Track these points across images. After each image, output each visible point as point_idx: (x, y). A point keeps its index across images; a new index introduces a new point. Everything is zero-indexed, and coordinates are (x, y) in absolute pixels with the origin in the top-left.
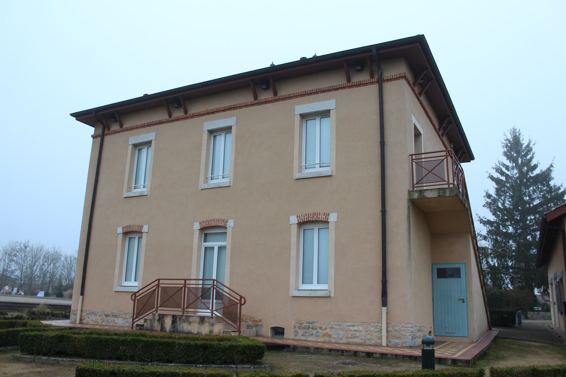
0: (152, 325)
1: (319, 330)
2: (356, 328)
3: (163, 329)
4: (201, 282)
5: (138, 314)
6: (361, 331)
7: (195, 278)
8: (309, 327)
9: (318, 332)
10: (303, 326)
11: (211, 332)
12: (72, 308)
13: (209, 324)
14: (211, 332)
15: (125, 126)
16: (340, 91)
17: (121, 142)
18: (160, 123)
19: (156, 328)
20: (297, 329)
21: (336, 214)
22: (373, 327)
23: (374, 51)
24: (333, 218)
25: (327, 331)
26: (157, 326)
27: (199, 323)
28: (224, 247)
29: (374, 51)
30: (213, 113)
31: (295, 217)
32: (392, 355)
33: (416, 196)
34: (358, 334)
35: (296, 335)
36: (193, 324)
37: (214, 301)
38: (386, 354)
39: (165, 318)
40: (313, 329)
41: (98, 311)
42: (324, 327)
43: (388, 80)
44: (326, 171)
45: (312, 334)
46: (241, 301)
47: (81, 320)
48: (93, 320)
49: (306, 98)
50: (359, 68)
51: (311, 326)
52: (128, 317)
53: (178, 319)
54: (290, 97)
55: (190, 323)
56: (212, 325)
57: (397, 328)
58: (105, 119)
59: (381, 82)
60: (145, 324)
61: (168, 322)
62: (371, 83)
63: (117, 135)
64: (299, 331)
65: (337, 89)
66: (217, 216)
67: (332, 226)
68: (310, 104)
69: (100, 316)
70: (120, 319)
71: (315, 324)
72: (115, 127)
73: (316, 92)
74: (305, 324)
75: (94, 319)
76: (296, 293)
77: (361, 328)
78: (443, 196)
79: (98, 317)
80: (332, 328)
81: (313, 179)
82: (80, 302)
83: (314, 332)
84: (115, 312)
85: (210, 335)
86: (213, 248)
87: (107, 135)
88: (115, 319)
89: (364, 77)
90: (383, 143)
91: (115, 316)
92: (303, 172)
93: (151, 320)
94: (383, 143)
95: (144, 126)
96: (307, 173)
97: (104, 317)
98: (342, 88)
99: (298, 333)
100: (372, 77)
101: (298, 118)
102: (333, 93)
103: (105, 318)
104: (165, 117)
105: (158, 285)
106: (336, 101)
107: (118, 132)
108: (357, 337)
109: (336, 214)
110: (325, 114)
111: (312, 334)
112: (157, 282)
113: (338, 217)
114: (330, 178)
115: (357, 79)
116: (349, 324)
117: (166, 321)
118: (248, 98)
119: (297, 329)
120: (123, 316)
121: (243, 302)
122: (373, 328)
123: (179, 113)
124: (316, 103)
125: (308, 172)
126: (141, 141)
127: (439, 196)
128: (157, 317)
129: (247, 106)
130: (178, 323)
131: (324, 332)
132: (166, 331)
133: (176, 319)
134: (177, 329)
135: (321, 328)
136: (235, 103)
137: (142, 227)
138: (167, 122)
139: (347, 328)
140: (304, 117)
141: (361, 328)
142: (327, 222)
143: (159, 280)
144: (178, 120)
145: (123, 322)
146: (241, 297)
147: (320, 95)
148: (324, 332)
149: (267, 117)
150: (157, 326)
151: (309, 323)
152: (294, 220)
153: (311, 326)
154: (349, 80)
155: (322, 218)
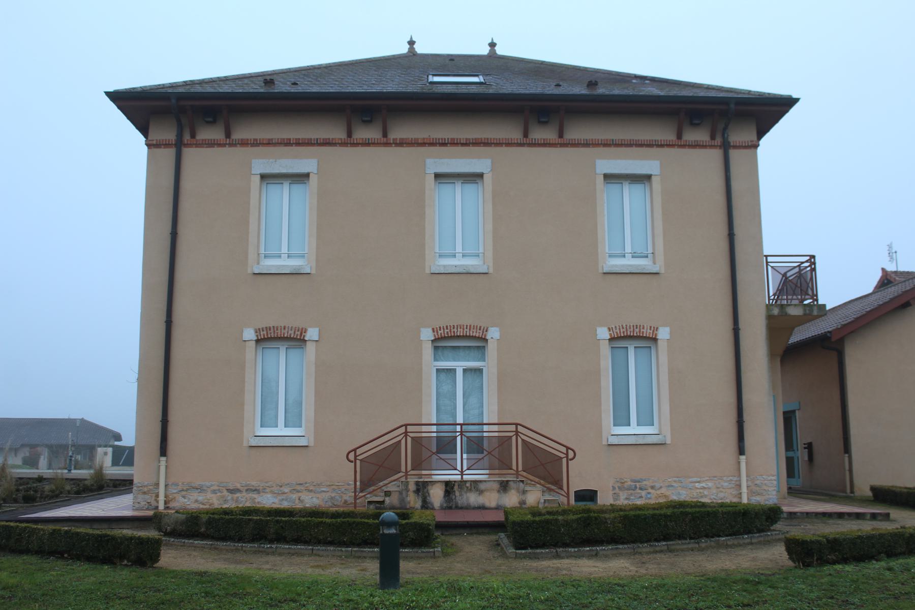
0: (402, 500)
1: (650, 490)
2: (703, 485)
3: (426, 505)
4: (458, 428)
5: (366, 483)
6: (709, 488)
7: (496, 422)
8: (636, 487)
9: (649, 493)
10: (626, 485)
11: (523, 503)
12: (135, 481)
13: (518, 492)
14: (523, 503)
15: (237, 135)
16: (666, 150)
17: (207, 165)
18: (327, 143)
19: (412, 504)
20: (617, 491)
21: (667, 329)
22: (726, 482)
24: (663, 334)
25: (663, 491)
26: (414, 501)
27: (499, 491)
28: (479, 371)
29: (174, 101)
30: (444, 144)
31: (606, 329)
32: (802, 513)
33: (776, 311)
34: (706, 493)
35: (615, 500)
36: (487, 494)
37: (465, 456)
38: (795, 513)
39: (429, 487)
40: (641, 489)
41: (208, 484)
42: (657, 485)
43: (735, 147)
44: (643, 264)
45: (641, 497)
46: (567, 454)
47: (166, 503)
48: (196, 501)
49: (613, 150)
50: (210, 119)
51: (638, 485)
52: (286, 491)
53: (456, 488)
54: (587, 144)
55: (481, 492)
56: (524, 492)
57: (758, 482)
58: (171, 115)
59: (726, 147)
60: (387, 499)
61: (437, 495)
62: (712, 147)
63: (216, 150)
64: (621, 494)
65: (662, 146)
66: (467, 320)
67: (662, 345)
68: (619, 161)
69: (214, 492)
70: (269, 496)
71: (645, 483)
72: (213, 133)
73: (630, 144)
74: (629, 483)
75: (200, 498)
76: (254, 442)
77: (710, 484)
78: (810, 315)
79: (209, 495)
80: (669, 486)
81: (630, 276)
82: (847, 459)
83: (643, 493)
84: (254, 483)
85: (520, 508)
86: (452, 371)
87: (188, 145)
88: (255, 496)
89: (700, 135)
90: (731, 236)
91: (256, 491)
92: (262, 263)
93: (400, 493)
94: (731, 236)
95: (287, 143)
96: (444, 266)
97: (225, 493)
98: (669, 146)
99: (618, 496)
100: (713, 137)
102: (655, 150)
103: (230, 497)
104: (671, 136)
105: (406, 433)
106: (661, 164)
107: (220, 145)
108: (706, 496)
109: (667, 329)
110: (302, 178)
111: (641, 497)
112: (403, 430)
113: (671, 333)
114: (656, 276)
115: (691, 135)
116: (695, 479)
117: (431, 492)
118: (511, 131)
119: (617, 491)
120: (275, 489)
121: (571, 454)
122: (726, 484)
123: (538, 134)
124: (631, 162)
125: (270, 264)
126: (284, 171)
127: (805, 314)
128: (412, 487)
129: (509, 144)
130: (457, 494)
131: (658, 492)
132: (433, 509)
133: (453, 488)
134: (456, 503)
135: (652, 487)
136: (404, 136)
137: (303, 331)
138: (344, 144)
139: (691, 485)
140: (608, 177)
141: (710, 484)
142: (655, 340)
143: (406, 425)
145: (276, 501)
146: (568, 448)
147: (634, 149)
148: (658, 492)
149: (370, 168)
150: (414, 501)
151: (635, 481)
152: (603, 333)
153: (638, 485)
154: (679, 136)
155: (647, 332)
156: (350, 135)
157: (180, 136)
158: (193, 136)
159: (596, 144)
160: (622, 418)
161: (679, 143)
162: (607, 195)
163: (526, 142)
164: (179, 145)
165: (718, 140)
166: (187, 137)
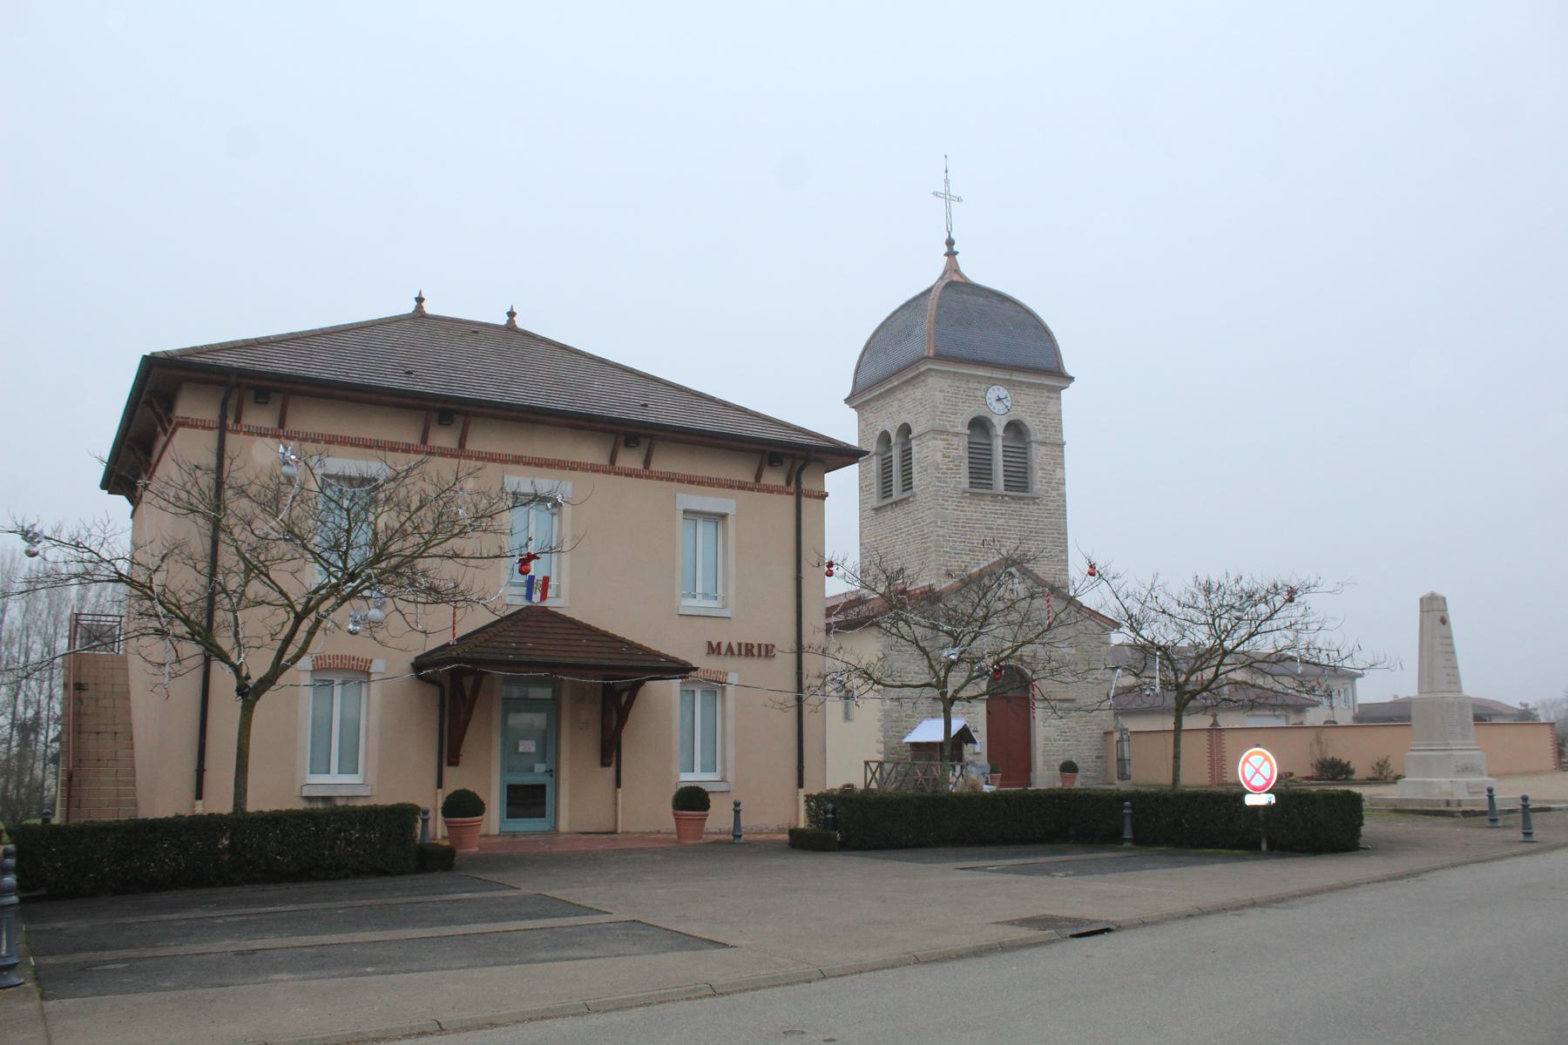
23: (233, 379)
54: (670, 478)
89: (774, 478)
100: (788, 484)
101: (680, 515)
102: (568, 473)
118: (744, 474)
123: (630, 460)
144: (771, 490)
156: (758, 479)
157: (223, 417)
158: (238, 420)
159: (682, 480)
160: (321, 764)
161: (757, 486)
162: (682, 527)
163: (611, 468)
164: (222, 430)
165: (793, 485)
166: (230, 422)
